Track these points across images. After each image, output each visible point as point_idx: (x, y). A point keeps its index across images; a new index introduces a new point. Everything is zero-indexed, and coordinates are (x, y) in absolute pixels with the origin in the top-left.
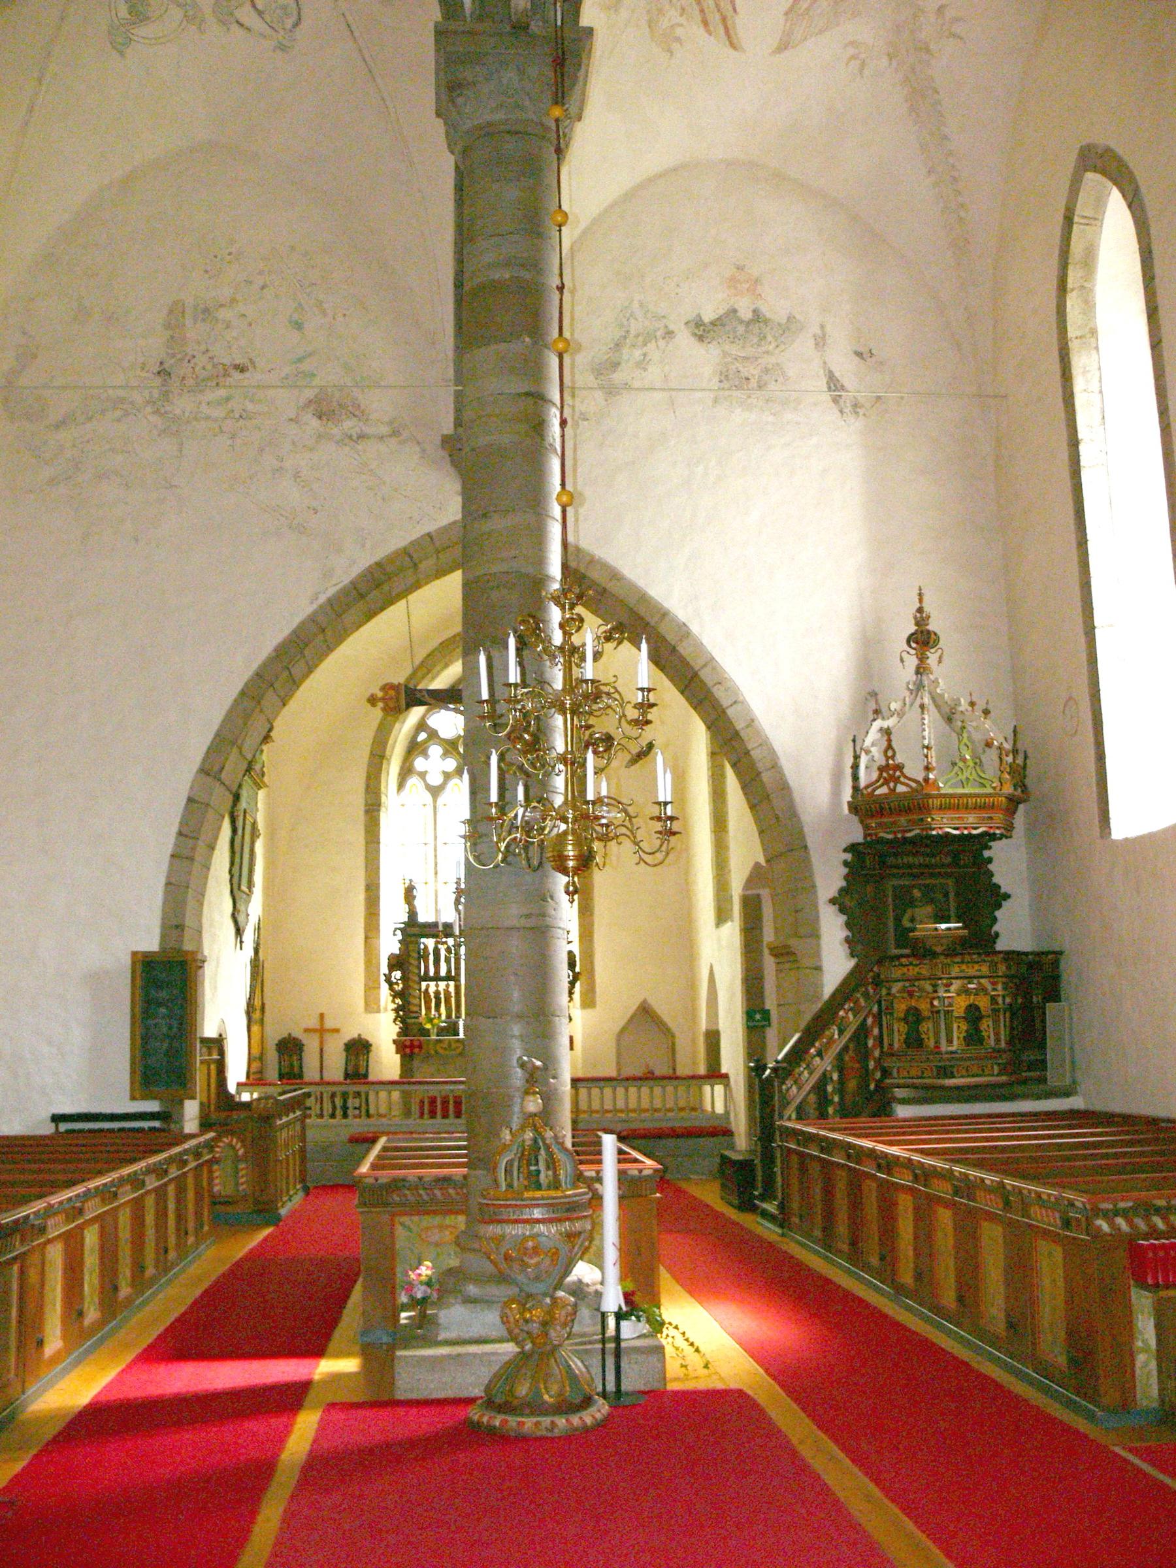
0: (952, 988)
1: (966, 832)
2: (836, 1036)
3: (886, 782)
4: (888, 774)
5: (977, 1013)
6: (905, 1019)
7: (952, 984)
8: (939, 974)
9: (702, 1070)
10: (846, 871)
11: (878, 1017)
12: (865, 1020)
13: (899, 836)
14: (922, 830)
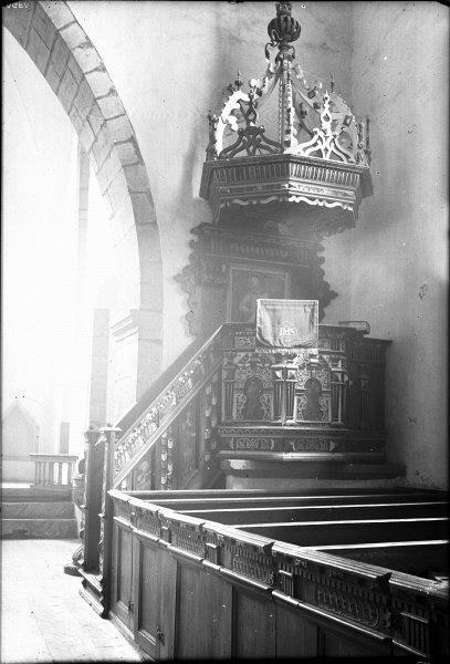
1: (321, 204)
3: (246, 147)
4: (249, 138)
6: (245, 391)
9: (56, 452)
13: (255, 202)
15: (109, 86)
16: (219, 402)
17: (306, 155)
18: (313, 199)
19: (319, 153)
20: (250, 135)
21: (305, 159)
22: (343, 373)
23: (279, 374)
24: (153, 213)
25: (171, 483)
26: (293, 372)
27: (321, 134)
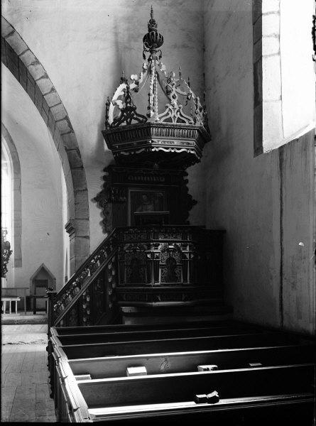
0: (160, 247)
1: (173, 151)
2: (89, 275)
5: (174, 264)
7: (159, 245)
8: (152, 239)
10: (103, 182)
11: (115, 265)
12: (107, 266)
14: (146, 148)
15: (51, 87)
16: (116, 274)
17: (161, 122)
18: (167, 149)
19: (170, 120)
20: (129, 111)
21: (161, 124)
22: (190, 253)
23: (149, 256)
24: (81, 161)
25: (89, 321)
26: (157, 254)
27: (171, 107)
